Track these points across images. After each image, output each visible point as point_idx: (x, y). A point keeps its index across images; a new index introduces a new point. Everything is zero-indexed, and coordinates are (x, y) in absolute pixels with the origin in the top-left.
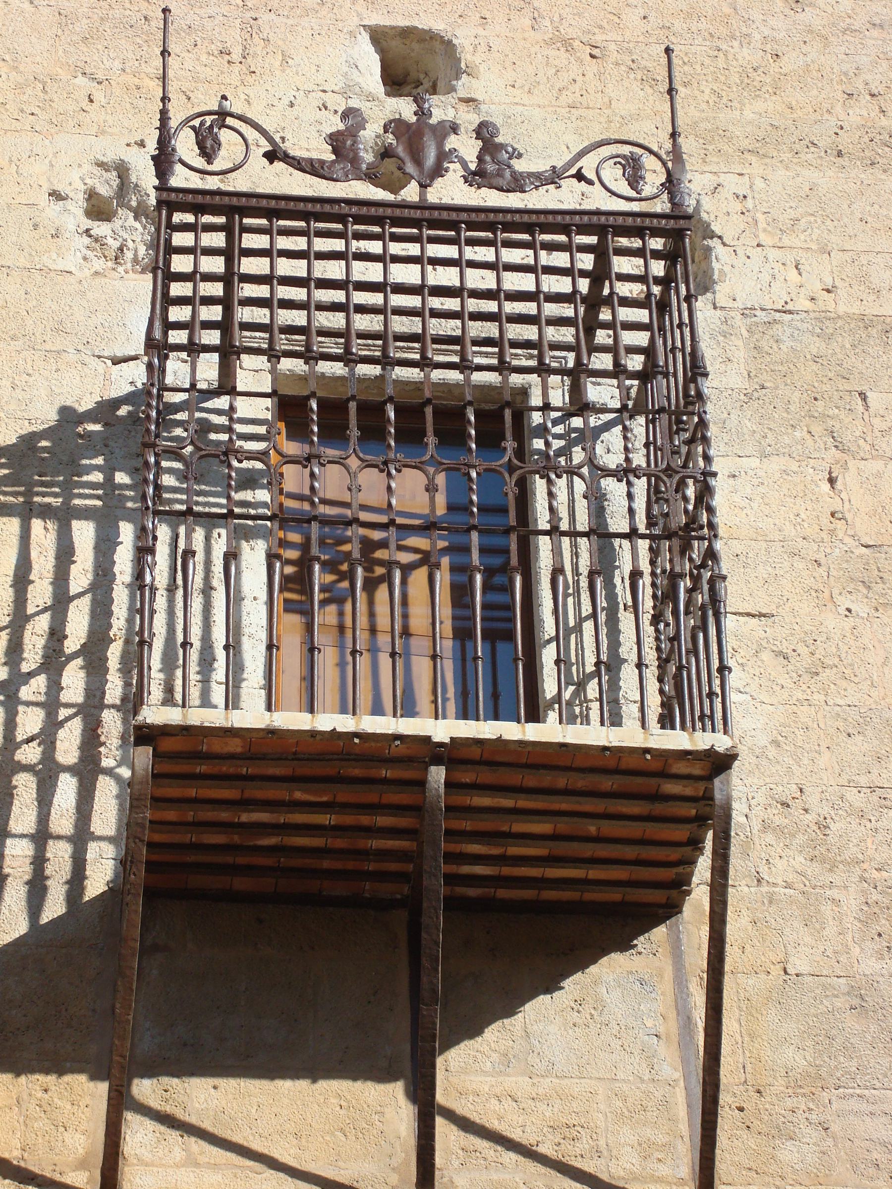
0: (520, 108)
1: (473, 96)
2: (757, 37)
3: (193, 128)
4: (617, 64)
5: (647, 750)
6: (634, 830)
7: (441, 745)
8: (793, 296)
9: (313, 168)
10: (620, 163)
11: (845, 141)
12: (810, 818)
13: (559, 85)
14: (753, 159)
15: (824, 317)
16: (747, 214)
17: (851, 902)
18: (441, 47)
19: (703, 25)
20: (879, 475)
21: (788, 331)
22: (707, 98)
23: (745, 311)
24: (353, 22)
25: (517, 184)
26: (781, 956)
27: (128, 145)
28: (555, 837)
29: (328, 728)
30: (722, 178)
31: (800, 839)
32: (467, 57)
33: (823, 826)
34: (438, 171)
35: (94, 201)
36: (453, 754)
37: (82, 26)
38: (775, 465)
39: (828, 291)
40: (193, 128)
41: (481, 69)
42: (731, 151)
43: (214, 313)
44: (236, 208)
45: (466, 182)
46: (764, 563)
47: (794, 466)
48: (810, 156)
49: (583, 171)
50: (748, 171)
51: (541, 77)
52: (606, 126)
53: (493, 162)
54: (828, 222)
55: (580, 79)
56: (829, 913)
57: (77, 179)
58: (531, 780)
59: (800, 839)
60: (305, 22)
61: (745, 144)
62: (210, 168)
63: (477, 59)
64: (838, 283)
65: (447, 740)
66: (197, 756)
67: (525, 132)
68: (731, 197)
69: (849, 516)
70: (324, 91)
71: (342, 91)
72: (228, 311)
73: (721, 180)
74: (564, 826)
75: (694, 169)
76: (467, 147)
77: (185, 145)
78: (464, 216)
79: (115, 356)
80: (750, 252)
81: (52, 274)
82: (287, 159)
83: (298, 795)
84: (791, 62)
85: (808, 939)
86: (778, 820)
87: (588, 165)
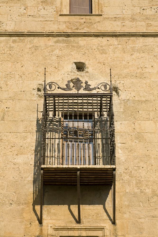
2: (126, 60)
4: (107, 65)
5: (105, 168)
6: (105, 176)
7: (79, 169)
8: (130, 98)
9: (64, 89)
11: (137, 75)
12: (129, 171)
14: (125, 78)
15: (134, 100)
17: (134, 182)
18: (83, 64)
19: (119, 59)
20: (140, 123)
21: (129, 103)
24: (72, 62)
25: (91, 90)
26: (125, 190)
28: (95, 178)
29: (65, 167)
30: (121, 81)
31: (128, 174)
32: (87, 66)
33: (131, 172)
34: (80, 89)
36: (81, 169)
37: (37, 65)
38: (126, 122)
39: (134, 97)
43: (56, 101)
44: (54, 96)
46: (125, 136)
47: (129, 122)
48: (133, 77)
51: (97, 68)
53: (87, 87)
54: (135, 87)
55: (102, 68)
56: (131, 184)
57: (36, 87)
58: (91, 172)
59: (128, 174)
60: (66, 62)
61: (124, 76)
62: (50, 90)
63: (89, 66)
64: (136, 95)
65: (79, 168)
66: (49, 171)
69: (136, 129)
74: (96, 176)
76: (84, 85)
77: (48, 87)
78: (83, 95)
80: (124, 92)
82: (60, 88)
83: (62, 174)
84: (130, 64)
85: (129, 187)
86: (125, 172)
87: (99, 87)
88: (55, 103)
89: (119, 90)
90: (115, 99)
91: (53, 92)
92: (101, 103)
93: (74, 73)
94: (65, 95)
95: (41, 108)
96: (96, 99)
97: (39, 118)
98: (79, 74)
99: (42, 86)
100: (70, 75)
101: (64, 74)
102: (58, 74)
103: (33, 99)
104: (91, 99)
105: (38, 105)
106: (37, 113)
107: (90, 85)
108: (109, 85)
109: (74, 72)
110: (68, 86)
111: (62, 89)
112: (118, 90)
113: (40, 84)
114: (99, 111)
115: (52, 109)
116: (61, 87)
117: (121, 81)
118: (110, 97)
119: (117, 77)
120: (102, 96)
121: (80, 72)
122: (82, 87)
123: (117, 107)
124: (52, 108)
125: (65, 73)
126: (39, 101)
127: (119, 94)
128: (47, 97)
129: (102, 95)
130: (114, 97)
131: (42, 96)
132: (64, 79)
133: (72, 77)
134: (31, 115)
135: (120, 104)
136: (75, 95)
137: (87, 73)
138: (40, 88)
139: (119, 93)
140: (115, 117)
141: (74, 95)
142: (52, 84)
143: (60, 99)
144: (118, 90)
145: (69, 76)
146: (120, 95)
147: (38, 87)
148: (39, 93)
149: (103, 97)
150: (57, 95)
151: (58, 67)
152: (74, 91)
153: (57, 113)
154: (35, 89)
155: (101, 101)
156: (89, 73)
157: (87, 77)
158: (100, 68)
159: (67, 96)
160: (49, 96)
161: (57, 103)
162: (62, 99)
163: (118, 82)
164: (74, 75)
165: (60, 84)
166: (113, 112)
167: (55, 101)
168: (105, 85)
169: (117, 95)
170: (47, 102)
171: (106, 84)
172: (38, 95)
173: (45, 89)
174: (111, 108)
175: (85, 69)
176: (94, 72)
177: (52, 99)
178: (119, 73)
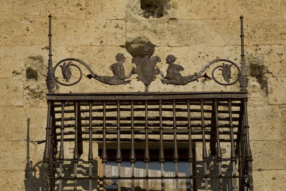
0: (193, 21)
1: (175, 17)
3: (61, 66)
9: (106, 81)
10: (221, 69)
13: (209, 10)
16: (282, 62)
22: (268, 11)
23: (281, 106)
25: (184, 81)
27: (42, 49)
30: (273, 47)
34: (153, 79)
35: (30, 72)
40: (61, 66)
41: (179, 5)
42: (277, 34)
44: (77, 101)
45: (162, 82)
49: (207, 74)
50: (284, 43)
52: (227, 26)
53: (174, 75)
57: (21, 66)
62: (68, 83)
67: (195, 32)
68: (276, 55)
70: (118, 19)
71: (125, 18)
72: (79, 122)
73: (272, 48)
75: (262, 43)
76: (163, 67)
77: (58, 73)
79: (39, 141)
81: (15, 108)
88: (80, 119)
89: (267, 75)
90: (256, 103)
91: (75, 89)
92: (213, 119)
93: (135, 24)
94: (110, 98)
95: (39, 129)
96: (198, 107)
97: (31, 162)
98: (149, 26)
99: (40, 64)
100: (124, 29)
101: (105, 26)
102: (88, 26)
103: (13, 103)
104: (184, 107)
105: (30, 122)
106: (26, 147)
107: (180, 67)
108: (236, 66)
109: (135, 21)
110: (119, 70)
111: (102, 80)
112: (265, 75)
113: (34, 58)
114: (207, 141)
115: (72, 136)
116: (98, 75)
117: (273, 47)
118: (239, 102)
119: (260, 33)
120: (215, 100)
121: (151, 17)
122: (157, 72)
123: (263, 128)
124: (71, 119)
125: (108, 21)
126: (32, 109)
127: (267, 87)
128: (56, 103)
129: (216, 96)
130: (253, 95)
131: (41, 92)
132: (104, 41)
133: (128, 35)
134: (9, 154)
135: (272, 116)
136: (137, 98)
137: (171, 22)
138: (34, 68)
139: (268, 82)
140: (255, 164)
141: (134, 98)
142: (72, 65)
143: (94, 108)
144: (265, 75)
145: (121, 31)
146: (271, 88)
147: (28, 66)
148: (33, 84)
149: (221, 102)
150: (87, 98)
151: (87, 5)
152: (137, 86)
153: (86, 145)
154: (19, 71)
155: (213, 112)
156: (179, 22)
157: (172, 33)
158: (211, 5)
159: (116, 101)
160: (63, 101)
161: (87, 118)
162: (101, 107)
163: (265, 49)
164: (134, 30)
165: (92, 55)
166: (248, 148)
167: (79, 115)
168: (226, 66)
169: (262, 88)
170: (58, 116)
171: (229, 64)
172: (27, 91)
173: (50, 79)
174: (244, 135)
175: (168, 11)
176: (192, 19)
177: (72, 108)
178: (268, 20)
